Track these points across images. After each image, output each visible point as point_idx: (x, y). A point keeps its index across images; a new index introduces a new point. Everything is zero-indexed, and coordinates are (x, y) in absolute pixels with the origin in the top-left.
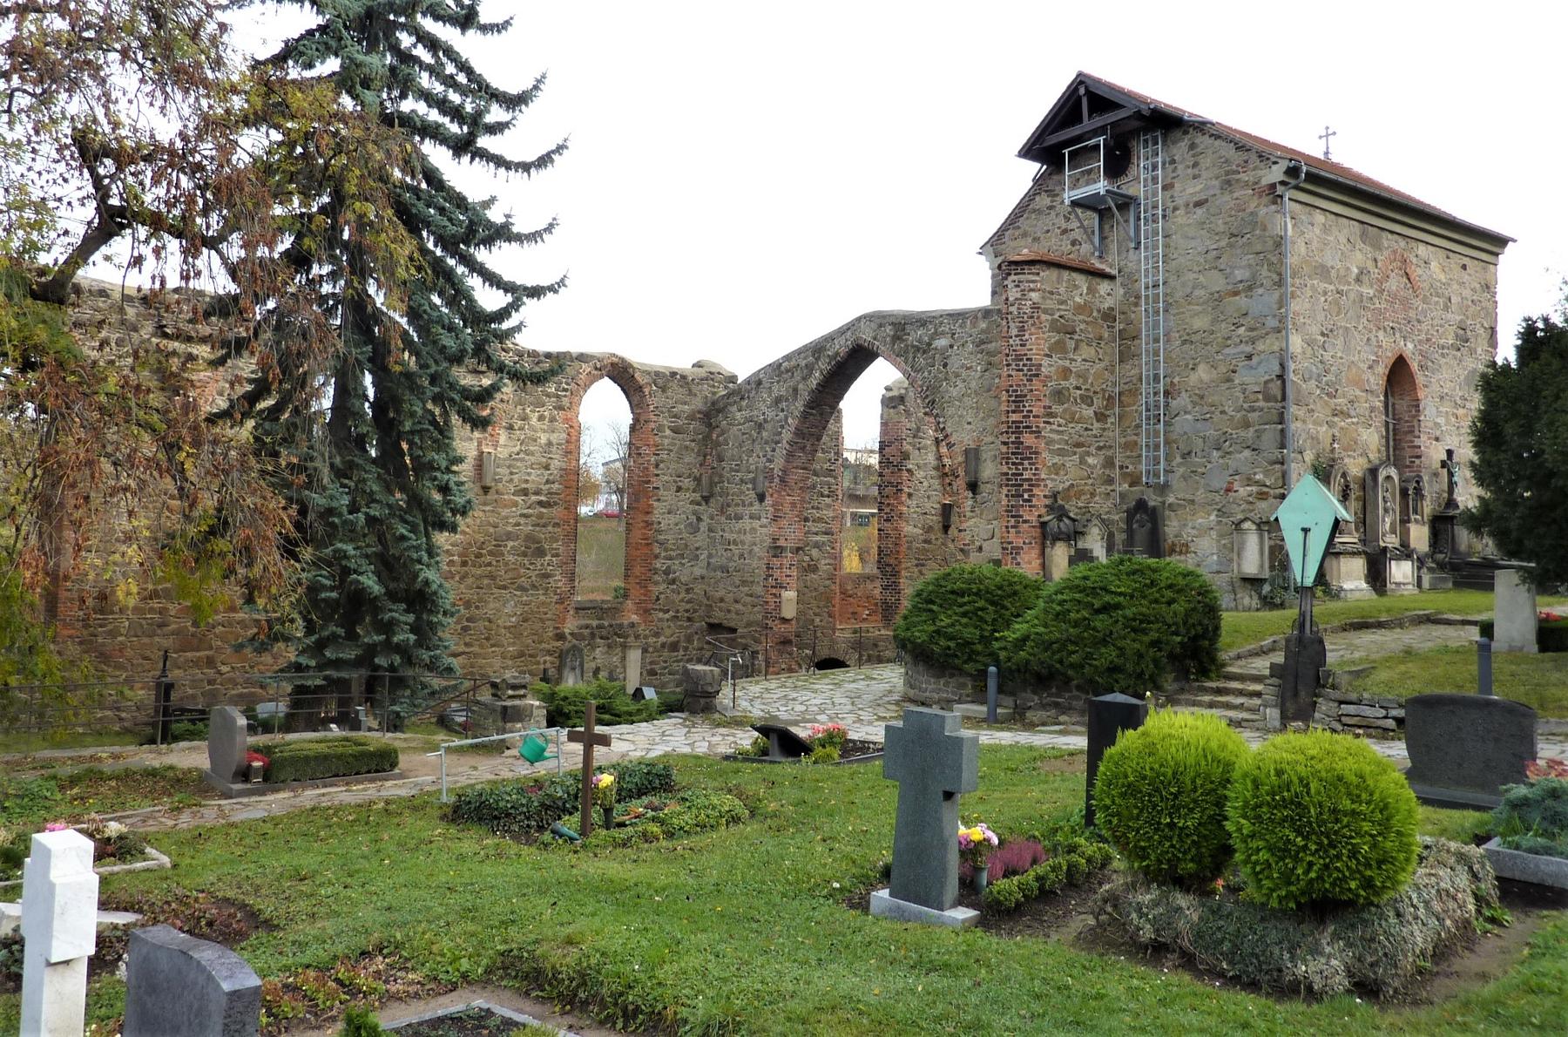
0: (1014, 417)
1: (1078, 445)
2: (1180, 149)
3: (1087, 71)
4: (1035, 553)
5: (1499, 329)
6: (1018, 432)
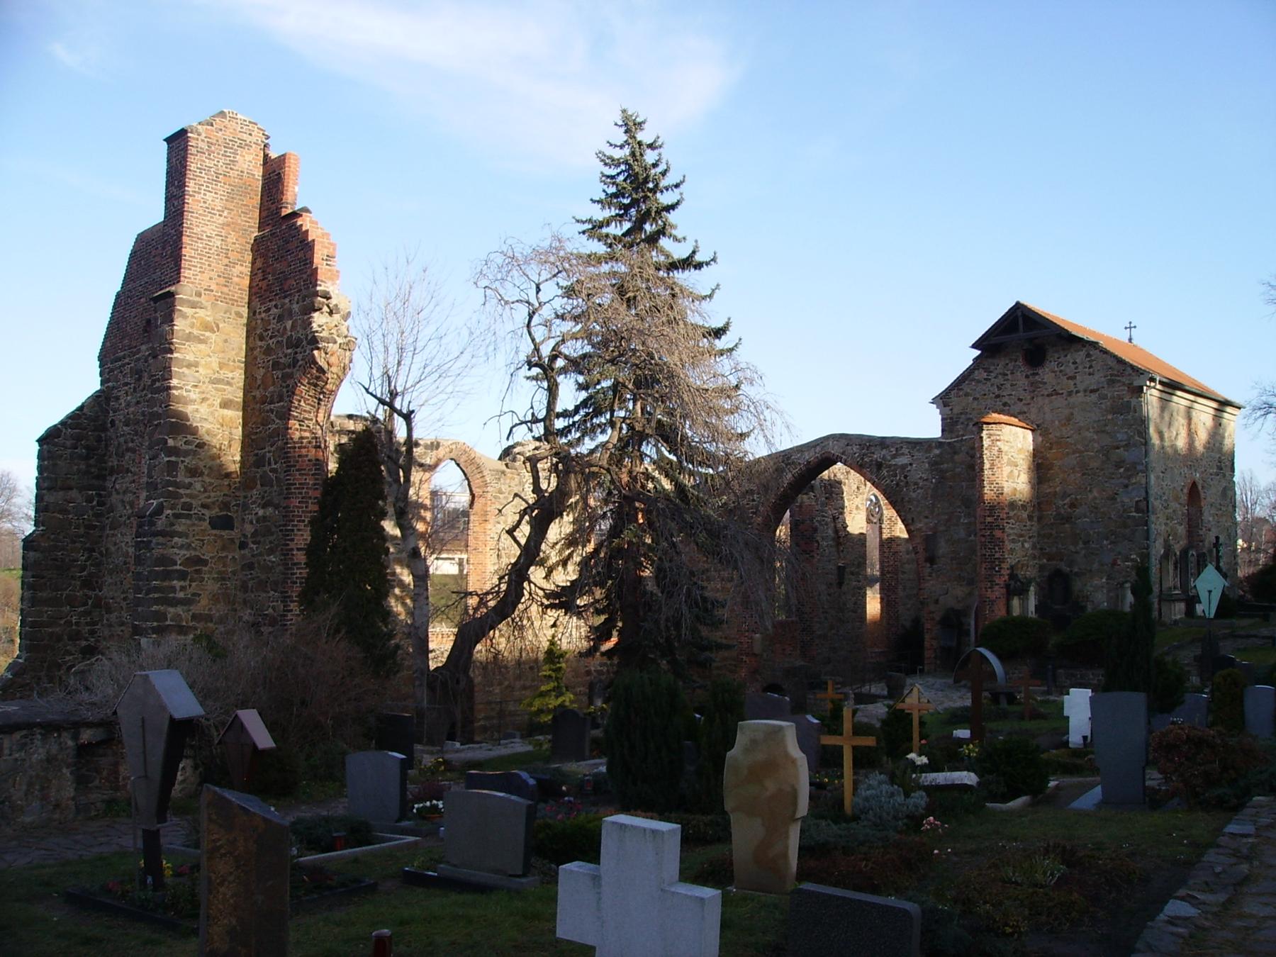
0: (989, 519)
1: (1021, 536)
2: (1080, 356)
3: (1022, 302)
4: (1003, 601)
5: (1236, 461)
6: (991, 529)
